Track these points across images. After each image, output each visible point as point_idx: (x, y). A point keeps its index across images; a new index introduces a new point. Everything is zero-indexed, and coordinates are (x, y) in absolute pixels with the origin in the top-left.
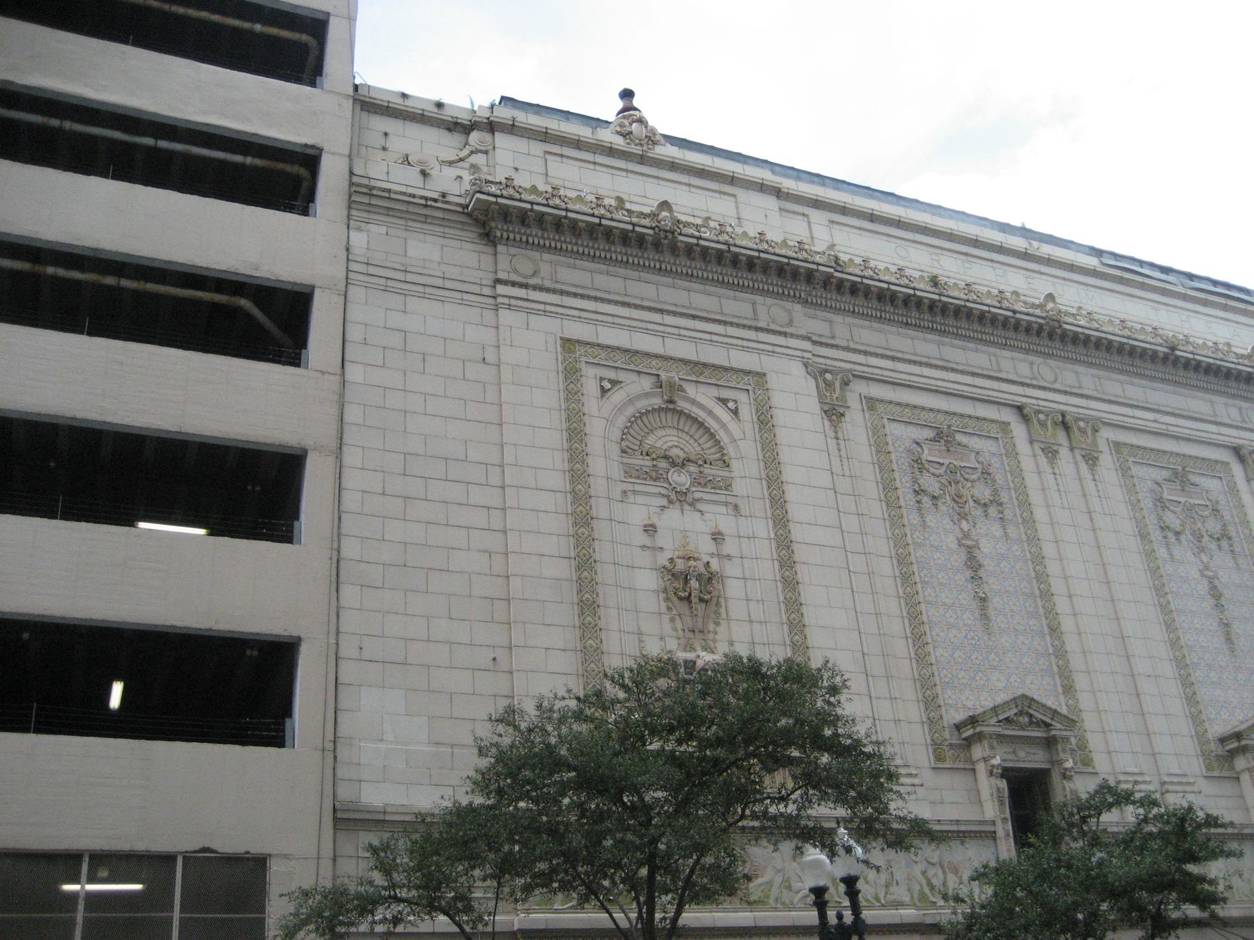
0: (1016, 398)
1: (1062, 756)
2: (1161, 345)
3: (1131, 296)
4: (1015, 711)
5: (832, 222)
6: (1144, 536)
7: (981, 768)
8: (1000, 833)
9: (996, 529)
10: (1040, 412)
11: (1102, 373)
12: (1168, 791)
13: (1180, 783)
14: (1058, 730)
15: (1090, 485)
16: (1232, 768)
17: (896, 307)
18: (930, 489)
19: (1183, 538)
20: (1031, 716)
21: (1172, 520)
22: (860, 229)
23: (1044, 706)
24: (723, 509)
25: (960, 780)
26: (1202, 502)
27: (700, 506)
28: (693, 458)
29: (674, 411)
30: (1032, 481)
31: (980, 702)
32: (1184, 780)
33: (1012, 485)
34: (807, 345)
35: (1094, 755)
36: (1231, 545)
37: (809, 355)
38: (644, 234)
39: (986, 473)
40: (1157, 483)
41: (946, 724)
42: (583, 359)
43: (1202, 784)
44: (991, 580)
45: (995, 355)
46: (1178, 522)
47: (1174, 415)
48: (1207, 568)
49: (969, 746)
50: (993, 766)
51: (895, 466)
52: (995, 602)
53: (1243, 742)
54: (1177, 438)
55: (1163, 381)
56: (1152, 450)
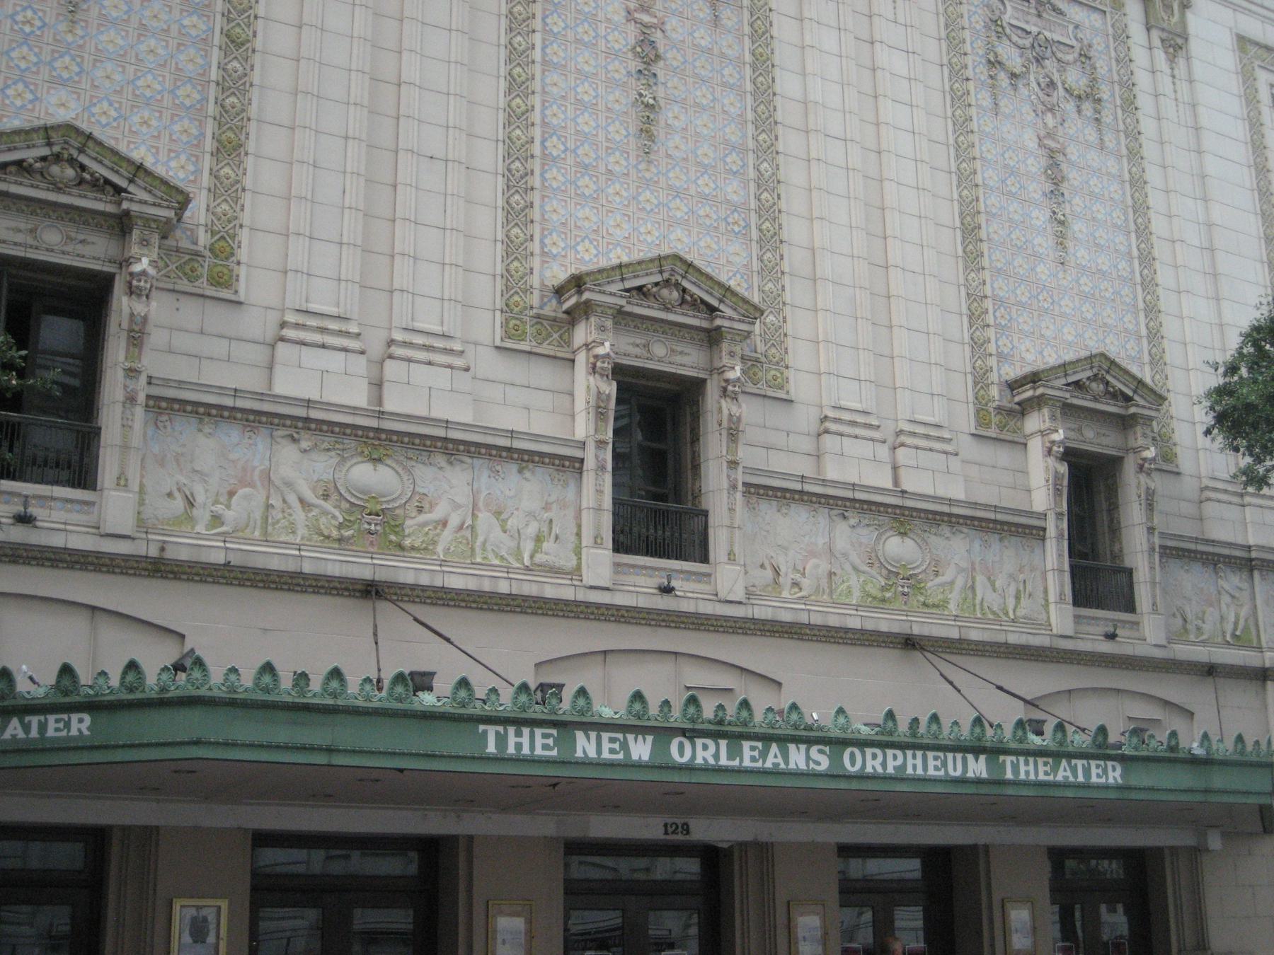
1: (726, 360)
4: (1089, 373)
6: (957, 73)
7: (581, 358)
8: (1051, 531)
12: (827, 431)
13: (323, 330)
14: (728, 318)
18: (1008, 63)
20: (83, 168)
21: (1013, 59)
23: (115, 153)
25: (544, 374)
26: (1068, 42)
30: (1142, 79)
32: (439, 343)
35: (1178, 450)
39: (1085, 56)
41: (536, 283)
43: (488, 363)
44: (1077, 200)
50: (1053, 442)
52: (669, 114)
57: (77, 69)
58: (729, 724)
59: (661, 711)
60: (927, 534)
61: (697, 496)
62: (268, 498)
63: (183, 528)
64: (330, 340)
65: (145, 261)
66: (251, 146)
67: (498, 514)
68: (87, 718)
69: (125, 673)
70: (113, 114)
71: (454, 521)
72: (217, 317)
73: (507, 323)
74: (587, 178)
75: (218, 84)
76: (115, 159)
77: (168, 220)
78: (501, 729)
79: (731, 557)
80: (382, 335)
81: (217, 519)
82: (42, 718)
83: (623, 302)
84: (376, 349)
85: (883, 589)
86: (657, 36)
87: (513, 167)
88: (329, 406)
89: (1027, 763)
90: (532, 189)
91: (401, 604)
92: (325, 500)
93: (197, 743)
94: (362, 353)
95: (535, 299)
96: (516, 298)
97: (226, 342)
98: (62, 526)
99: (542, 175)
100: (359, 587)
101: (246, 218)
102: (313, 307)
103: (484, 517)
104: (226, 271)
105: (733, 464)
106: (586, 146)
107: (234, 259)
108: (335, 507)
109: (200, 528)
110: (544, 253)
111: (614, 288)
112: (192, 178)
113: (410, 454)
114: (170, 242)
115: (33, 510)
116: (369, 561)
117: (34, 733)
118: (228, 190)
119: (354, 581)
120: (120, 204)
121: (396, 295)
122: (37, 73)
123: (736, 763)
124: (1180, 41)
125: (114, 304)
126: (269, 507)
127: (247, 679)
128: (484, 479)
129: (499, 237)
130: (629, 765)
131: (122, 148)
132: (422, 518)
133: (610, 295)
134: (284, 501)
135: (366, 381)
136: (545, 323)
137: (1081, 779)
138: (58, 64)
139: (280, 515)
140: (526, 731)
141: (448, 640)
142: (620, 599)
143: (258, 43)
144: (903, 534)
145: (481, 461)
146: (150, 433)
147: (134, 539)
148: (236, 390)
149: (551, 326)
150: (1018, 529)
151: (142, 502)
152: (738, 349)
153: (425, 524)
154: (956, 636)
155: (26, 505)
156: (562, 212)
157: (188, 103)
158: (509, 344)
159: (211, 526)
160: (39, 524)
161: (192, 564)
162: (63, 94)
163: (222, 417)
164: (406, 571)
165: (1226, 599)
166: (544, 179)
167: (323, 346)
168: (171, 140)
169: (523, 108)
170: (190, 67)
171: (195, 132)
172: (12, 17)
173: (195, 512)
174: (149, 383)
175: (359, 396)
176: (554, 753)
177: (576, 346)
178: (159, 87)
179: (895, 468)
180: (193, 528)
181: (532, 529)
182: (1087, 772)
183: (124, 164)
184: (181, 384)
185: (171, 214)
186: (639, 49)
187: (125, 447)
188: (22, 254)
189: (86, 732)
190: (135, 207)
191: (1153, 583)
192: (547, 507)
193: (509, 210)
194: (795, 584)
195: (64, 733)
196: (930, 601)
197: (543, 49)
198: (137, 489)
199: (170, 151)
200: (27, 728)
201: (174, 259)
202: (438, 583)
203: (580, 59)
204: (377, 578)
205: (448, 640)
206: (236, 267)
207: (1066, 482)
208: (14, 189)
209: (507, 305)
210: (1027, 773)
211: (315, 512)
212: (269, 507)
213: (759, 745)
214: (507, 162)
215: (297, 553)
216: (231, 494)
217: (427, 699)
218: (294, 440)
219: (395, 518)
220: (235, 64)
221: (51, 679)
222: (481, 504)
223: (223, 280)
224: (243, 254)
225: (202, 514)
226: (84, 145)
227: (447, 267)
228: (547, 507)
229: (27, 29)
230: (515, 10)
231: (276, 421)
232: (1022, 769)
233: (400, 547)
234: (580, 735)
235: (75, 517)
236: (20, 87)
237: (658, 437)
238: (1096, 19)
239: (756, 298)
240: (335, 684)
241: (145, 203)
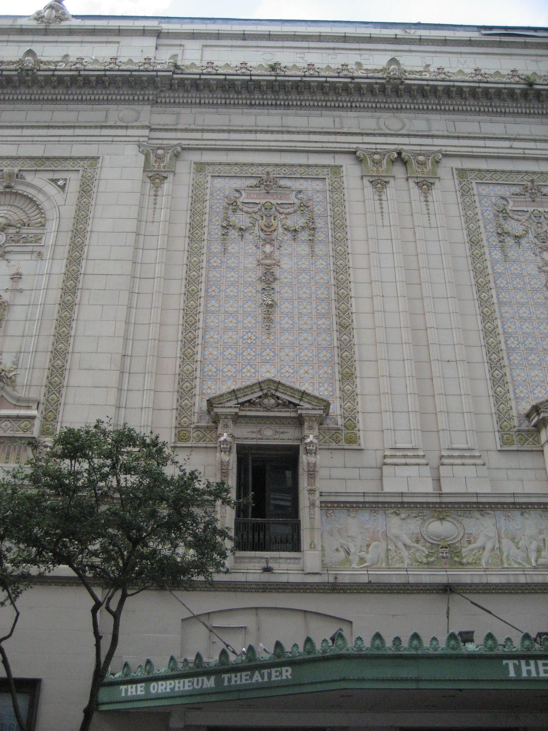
2: (517, 83)
6: (474, 242)
9: (303, 249)
13: (405, 456)
17: (504, 100)
19: (523, 242)
20: (278, 398)
22: (232, 46)
23: (247, 387)
24: (28, 257)
25: (527, 461)
27: (8, 257)
28: (13, 223)
29: (11, 193)
32: (467, 454)
34: (146, 132)
40: (503, 198)
42: (474, 182)
43: (495, 459)
45: (340, 117)
46: (521, 228)
49: (539, 431)
51: (480, 217)
54: (537, 159)
57: (273, 354)
58: (405, 649)
59: (394, 644)
60: (461, 518)
62: (387, 546)
63: (346, 566)
65: (311, 436)
66: (358, 373)
67: (513, 539)
68: (289, 669)
69: (305, 644)
70: (292, 371)
71: (489, 546)
72: (351, 458)
73: (503, 437)
74: (533, 355)
75: (338, 348)
76: (292, 391)
77: (321, 416)
78: (516, 662)
80: (437, 455)
81: (362, 560)
82: (269, 670)
83: (237, 410)
84: (435, 462)
87: (492, 357)
88: (413, 494)
90: (504, 366)
91: (465, 595)
92: (417, 543)
93: (344, 680)
94: (427, 465)
95: (516, 422)
96: (505, 423)
97: (357, 470)
98: (286, 571)
99: (508, 358)
100: (441, 587)
101: (359, 408)
102: (399, 445)
104: (353, 435)
106: (530, 339)
107: (356, 429)
108: (423, 546)
109: (354, 565)
110: (516, 398)
112: (331, 394)
113: (460, 513)
114: (325, 426)
115: (271, 565)
116: (445, 573)
118: (349, 396)
119: (438, 585)
120: (297, 411)
121: (441, 433)
122: (255, 360)
125: (300, 460)
126: (388, 550)
127: (367, 643)
128: (502, 522)
129: (491, 394)
131: (297, 386)
133: (230, 408)
134: (396, 547)
135: (430, 479)
136: (523, 433)
138: (264, 354)
139: (394, 554)
141: (490, 612)
143: (355, 325)
145: (499, 512)
146: (324, 520)
147: (321, 574)
148: (364, 493)
149: (527, 435)
151: (323, 555)
153: (473, 550)
155: (267, 563)
156: (523, 375)
157: (325, 359)
158: (505, 448)
160: (274, 571)
161: (352, 584)
162: (268, 366)
163: (359, 507)
164: (465, 576)
166: (510, 361)
167: (406, 464)
168: (319, 378)
169: (492, 327)
170: (324, 342)
171: (330, 372)
172: (242, 337)
173: (351, 557)
174: (321, 495)
175: (428, 487)
177: (543, 443)
178: (311, 355)
180: (351, 565)
181: (534, 546)
183: (296, 393)
184: (337, 494)
185: (321, 412)
186: (263, 278)
187: (312, 529)
188: (256, 443)
189: (290, 677)
190: (304, 412)
192: (541, 532)
193: (494, 380)
195: (279, 678)
197: (497, 297)
198: (320, 549)
199: (319, 383)
201: (327, 434)
202: (484, 581)
203: (518, 297)
204: (450, 582)
205: (490, 612)
206: (358, 433)
208: (249, 414)
209: (501, 428)
210: (529, 672)
212: (388, 550)
213: (249, 673)
214: (489, 355)
215: (405, 573)
216: (368, 546)
217: (471, 647)
218: (397, 514)
219: (456, 548)
220: (345, 337)
221: (271, 650)
222: (503, 536)
223: (352, 440)
224: (360, 426)
225: (354, 558)
226: (277, 387)
227: (465, 414)
228: (541, 532)
229: (249, 341)
230: (479, 281)
231: (387, 506)
233: (461, 563)
235: (291, 566)
236: (249, 367)
238: (317, 185)
240: (415, 642)
241: (308, 409)
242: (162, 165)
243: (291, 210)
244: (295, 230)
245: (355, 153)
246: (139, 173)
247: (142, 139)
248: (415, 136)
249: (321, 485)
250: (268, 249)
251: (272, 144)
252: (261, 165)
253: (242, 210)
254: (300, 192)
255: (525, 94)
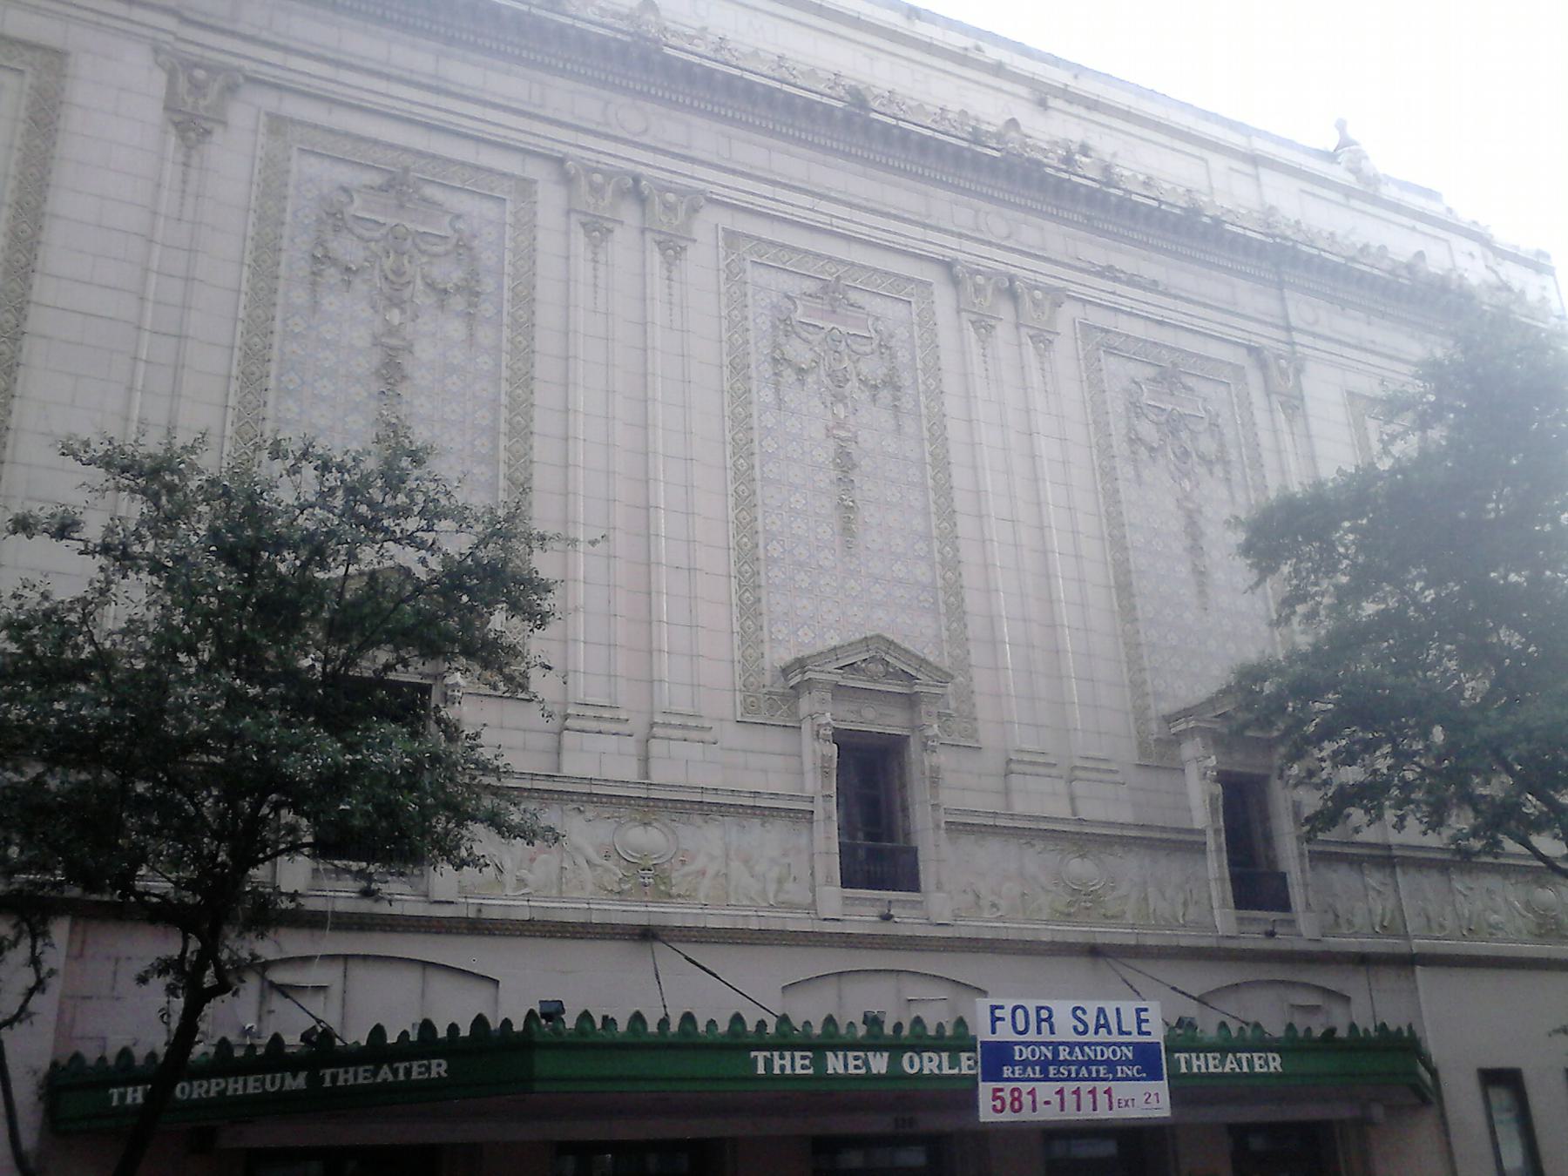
0: (558, 146)
1: (925, 720)
3: (799, 23)
5: (1303, 191)
6: (738, 368)
9: (456, 329)
10: (979, 272)
11: (733, 131)
15: (1035, 378)
16: (793, 712)
19: (810, 379)
21: (1147, 430)
23: (906, 651)
25: (776, 740)
31: (808, 641)
33: (508, 269)
36: (896, 399)
37: (170, 38)
38: (833, 108)
40: (789, 297)
41: (767, 666)
42: (749, 258)
46: (809, 355)
47: (1205, 305)
48: (1187, 498)
51: (750, 325)
53: (808, 675)
55: (847, 156)
56: (794, 250)
61: (907, 834)
64: (604, 726)
67: (746, 862)
71: (711, 872)
79: (939, 887)
81: (521, 882)
83: (837, 678)
85: (1069, 904)
86: (851, 448)
89: (1198, 1058)
91: (678, 946)
95: (767, 679)
102: (590, 700)
103: (736, 865)
105: (935, 806)
110: (772, 640)
111: (831, 667)
117: (401, 1077)
123: (956, 1071)
124: (1296, 403)
130: (870, 1078)
132: (686, 869)
133: (828, 673)
137: (1245, 1069)
140: (787, 1054)
142: (965, 933)
144: (1082, 856)
150: (1185, 845)
152: (934, 710)
153: (685, 876)
154: (1133, 942)
159: (516, 889)
165: (1372, 894)
175: (630, 771)
176: (811, 1071)
179: (1072, 799)
181: (774, 873)
182: (1250, 1062)
189: (444, 1074)
191: (1306, 885)
194: (994, 905)
196: (1109, 914)
200: (395, 1072)
207: (1220, 802)
211: (599, 870)
213: (371, 1067)
219: (664, 871)
225: (508, 878)
232: (1195, 1063)
233: (670, 896)
234: (830, 1055)
237: (877, 846)
238: (489, 209)
239: (946, 664)
242: (202, 103)
243: (440, 249)
244: (445, 291)
245: (561, 161)
246: (153, 112)
247: (161, 36)
248: (665, 153)
249: (948, 798)
250: (395, 316)
251: (416, 109)
252: (392, 146)
253: (351, 231)
254: (458, 217)
255: (848, 119)
